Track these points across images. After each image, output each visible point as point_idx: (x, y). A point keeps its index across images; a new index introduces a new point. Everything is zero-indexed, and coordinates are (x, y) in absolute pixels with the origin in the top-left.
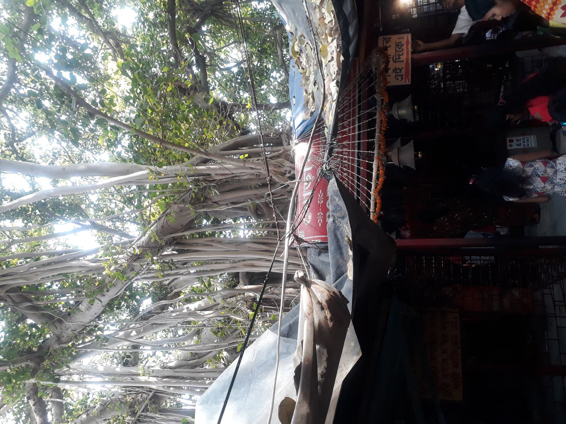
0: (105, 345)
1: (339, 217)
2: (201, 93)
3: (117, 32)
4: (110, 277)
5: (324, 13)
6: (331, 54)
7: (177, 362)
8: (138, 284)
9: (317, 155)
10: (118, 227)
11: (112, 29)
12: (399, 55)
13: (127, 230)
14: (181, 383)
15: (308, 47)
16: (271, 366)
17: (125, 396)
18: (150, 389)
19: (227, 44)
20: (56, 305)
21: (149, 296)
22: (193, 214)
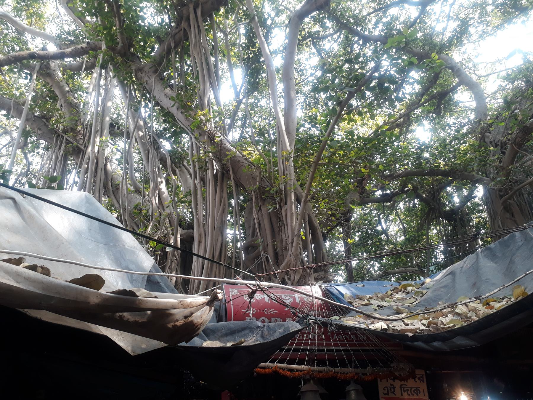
0: (131, 108)
1: (262, 333)
2: (358, 197)
3: (409, 125)
4: (195, 115)
5: (447, 316)
6: (412, 324)
7: (110, 171)
8: (185, 138)
9: (311, 308)
10: (237, 123)
11: (412, 121)
12: (408, 391)
13: (234, 130)
14: (91, 175)
15: (413, 300)
16: (120, 265)
17: (82, 124)
18: (87, 146)
19: (403, 221)
20: (170, 68)
21: (173, 148)
22: (251, 188)
